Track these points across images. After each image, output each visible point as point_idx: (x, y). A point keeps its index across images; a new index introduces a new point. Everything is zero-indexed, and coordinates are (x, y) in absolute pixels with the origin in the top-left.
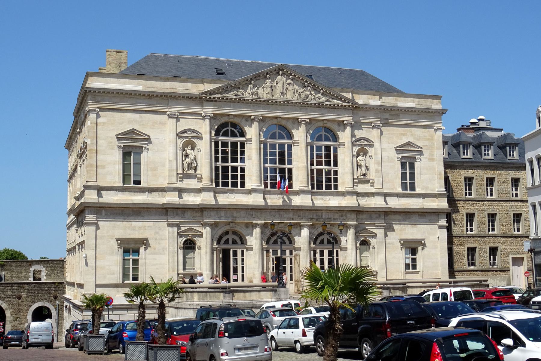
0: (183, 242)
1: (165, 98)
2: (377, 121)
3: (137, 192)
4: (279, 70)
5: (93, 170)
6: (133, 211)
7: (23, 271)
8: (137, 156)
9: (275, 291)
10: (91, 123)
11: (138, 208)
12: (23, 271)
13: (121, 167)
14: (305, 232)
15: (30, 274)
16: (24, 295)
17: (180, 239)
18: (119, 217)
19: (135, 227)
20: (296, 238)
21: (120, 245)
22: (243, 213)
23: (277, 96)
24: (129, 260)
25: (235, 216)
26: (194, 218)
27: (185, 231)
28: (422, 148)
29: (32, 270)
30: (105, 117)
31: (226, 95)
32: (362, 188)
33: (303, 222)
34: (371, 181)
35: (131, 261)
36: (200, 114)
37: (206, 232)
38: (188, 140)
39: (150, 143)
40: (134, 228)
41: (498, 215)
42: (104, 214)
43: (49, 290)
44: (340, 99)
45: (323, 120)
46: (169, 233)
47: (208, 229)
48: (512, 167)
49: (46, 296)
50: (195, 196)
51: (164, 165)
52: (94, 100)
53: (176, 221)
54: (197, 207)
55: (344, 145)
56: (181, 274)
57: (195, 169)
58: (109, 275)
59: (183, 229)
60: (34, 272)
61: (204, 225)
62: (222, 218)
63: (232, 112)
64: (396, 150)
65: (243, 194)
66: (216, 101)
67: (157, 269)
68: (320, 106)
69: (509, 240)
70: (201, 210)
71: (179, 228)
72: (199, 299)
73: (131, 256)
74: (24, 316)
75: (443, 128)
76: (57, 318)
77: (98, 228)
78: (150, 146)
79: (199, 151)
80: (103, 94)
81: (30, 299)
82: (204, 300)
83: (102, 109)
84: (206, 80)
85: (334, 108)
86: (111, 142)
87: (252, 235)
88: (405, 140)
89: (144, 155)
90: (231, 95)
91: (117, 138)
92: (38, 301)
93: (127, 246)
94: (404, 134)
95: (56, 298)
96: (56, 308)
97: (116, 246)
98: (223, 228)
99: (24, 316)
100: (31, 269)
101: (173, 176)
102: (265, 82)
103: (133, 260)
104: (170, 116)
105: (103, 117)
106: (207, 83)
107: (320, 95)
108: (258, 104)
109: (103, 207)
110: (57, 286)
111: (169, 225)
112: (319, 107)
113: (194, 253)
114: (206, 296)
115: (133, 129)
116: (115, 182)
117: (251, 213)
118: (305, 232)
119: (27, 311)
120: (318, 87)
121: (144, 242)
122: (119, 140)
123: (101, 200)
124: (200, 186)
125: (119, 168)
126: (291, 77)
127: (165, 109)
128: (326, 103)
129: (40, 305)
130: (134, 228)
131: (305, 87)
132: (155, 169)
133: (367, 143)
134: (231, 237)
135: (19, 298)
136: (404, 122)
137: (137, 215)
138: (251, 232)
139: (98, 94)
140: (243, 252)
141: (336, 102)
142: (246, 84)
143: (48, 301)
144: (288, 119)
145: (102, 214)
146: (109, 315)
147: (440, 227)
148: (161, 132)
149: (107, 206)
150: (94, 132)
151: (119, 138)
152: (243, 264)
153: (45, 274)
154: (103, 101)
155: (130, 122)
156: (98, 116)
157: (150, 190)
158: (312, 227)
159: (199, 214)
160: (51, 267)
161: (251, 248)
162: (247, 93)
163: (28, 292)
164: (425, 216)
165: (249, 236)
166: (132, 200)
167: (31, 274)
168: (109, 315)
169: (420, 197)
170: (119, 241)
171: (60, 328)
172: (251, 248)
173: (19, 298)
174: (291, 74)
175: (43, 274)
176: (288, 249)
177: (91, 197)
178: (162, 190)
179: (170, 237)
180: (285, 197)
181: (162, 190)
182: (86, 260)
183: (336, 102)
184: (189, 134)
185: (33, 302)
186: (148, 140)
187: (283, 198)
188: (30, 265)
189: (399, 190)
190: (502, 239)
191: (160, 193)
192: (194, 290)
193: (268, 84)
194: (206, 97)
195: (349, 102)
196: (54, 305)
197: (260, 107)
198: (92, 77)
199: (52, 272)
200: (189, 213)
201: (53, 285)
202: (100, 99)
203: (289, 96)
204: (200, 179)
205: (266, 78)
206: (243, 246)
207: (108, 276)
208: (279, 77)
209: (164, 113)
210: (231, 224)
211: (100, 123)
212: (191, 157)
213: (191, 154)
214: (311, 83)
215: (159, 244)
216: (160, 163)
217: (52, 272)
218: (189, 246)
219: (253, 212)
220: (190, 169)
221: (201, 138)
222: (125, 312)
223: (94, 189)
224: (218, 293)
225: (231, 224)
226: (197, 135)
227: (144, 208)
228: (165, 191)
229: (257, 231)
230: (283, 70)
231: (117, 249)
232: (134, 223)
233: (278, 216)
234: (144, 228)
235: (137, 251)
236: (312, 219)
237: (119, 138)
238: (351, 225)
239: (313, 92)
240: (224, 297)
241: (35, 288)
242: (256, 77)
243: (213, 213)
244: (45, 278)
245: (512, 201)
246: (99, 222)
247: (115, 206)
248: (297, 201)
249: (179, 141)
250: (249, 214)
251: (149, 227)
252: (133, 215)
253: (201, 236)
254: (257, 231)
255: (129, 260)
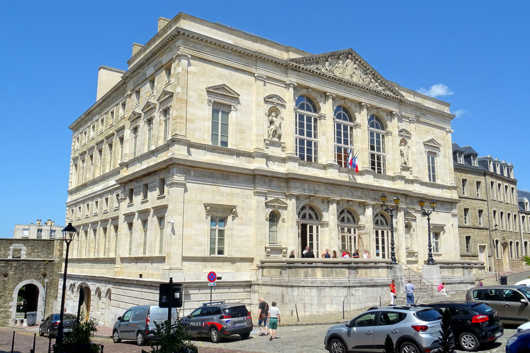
0: (269, 213)
1: (254, 59)
2: (412, 117)
3: (225, 154)
4: (349, 53)
5: (183, 123)
6: (222, 175)
7: (2, 249)
8: (225, 116)
9: (391, 268)
10: (182, 70)
11: (227, 172)
12: (2, 249)
13: (210, 124)
14: (369, 212)
15: (9, 252)
16: (11, 273)
17: (267, 210)
18: (208, 180)
19: (223, 193)
20: (361, 217)
21: (208, 212)
22: (322, 187)
23: (347, 77)
24: (215, 230)
25: (316, 189)
26: (280, 188)
27: (271, 202)
28: (440, 145)
29: (12, 248)
30: (197, 67)
31: (309, 67)
32: (406, 174)
33: (369, 201)
34: (410, 169)
35: (217, 231)
36: (284, 82)
37: (292, 204)
38: (274, 106)
39: (239, 103)
40: (222, 194)
41: (470, 210)
42: (192, 174)
43: (37, 268)
44: (392, 91)
45: (377, 108)
46: (258, 202)
47: (294, 200)
48: (476, 172)
49: (35, 274)
50: (279, 165)
51: (250, 129)
52: (186, 44)
53: (264, 190)
54: (285, 177)
55: (391, 134)
56: (268, 248)
57: (279, 137)
58: (196, 246)
59: (269, 199)
60: (14, 250)
61: (290, 197)
62: (306, 191)
63: (313, 85)
64: (424, 144)
65: (319, 168)
66: (299, 71)
67: (244, 241)
68: (377, 94)
69: (477, 231)
70: (288, 180)
71: (266, 199)
72: (323, 276)
73: (217, 226)
74: (9, 294)
75: (452, 131)
76: (44, 296)
77: (186, 191)
78: (238, 107)
79: (282, 118)
80: (196, 41)
81: (17, 276)
82: (329, 276)
83: (194, 57)
84: (291, 49)
85: (387, 97)
86: (201, 96)
87: (327, 211)
88: (429, 138)
89: (233, 115)
90: (313, 67)
91: (208, 91)
92: (25, 279)
93: (215, 214)
94: (428, 132)
95: (45, 275)
96: (44, 286)
97: (204, 212)
98: (304, 202)
99: (9, 294)
100: (10, 247)
101: (260, 141)
102: (337, 63)
103: (219, 231)
104: (257, 78)
105: (194, 65)
106: (291, 52)
107: (377, 84)
108: (333, 82)
109: (192, 167)
110: (47, 264)
111: (258, 194)
112: (376, 95)
113: (277, 226)
114: (332, 273)
115: (224, 85)
116: (204, 140)
117: (329, 188)
118: (369, 212)
119: (13, 289)
120: (377, 76)
121: (231, 210)
122: (210, 94)
123: (190, 158)
124: (284, 155)
125: (209, 124)
126: (357, 62)
127: (253, 70)
128: (383, 92)
129: (28, 283)
130: (222, 194)
131: (367, 74)
132: (242, 132)
133: (406, 135)
134: (307, 211)
135: (6, 275)
136: (428, 121)
137: (226, 179)
138: (326, 207)
139: (191, 39)
140: (317, 227)
141: (388, 93)
142: (323, 60)
143: (36, 279)
144: (352, 101)
145: (190, 175)
146: (211, 293)
147: (454, 215)
148: (252, 93)
149: (198, 165)
150: (185, 80)
151: (210, 92)
152: (317, 240)
153: (26, 252)
154: (195, 49)
155: (220, 77)
156: (189, 64)
157: (239, 154)
158: (374, 207)
159: (284, 185)
160: (32, 246)
161: (326, 224)
162: (325, 68)
163: (16, 269)
164: (444, 205)
165: (325, 212)
166: (221, 162)
167: (11, 253)
168: (211, 293)
169: (440, 188)
170: (208, 208)
171: (47, 306)
172: (326, 224)
173: (6, 275)
174: (357, 60)
175: (23, 252)
176: (352, 227)
177: (179, 152)
178: (249, 155)
179: (258, 207)
180: (351, 176)
181: (249, 155)
182: (173, 227)
183: (388, 93)
184: (274, 100)
185: (21, 280)
186: (236, 99)
187: (349, 177)
188: (10, 243)
189: (427, 180)
190: (473, 230)
191: (247, 158)
192: (311, 266)
193: (341, 65)
194: (293, 65)
195: (397, 95)
196: (42, 283)
197: (333, 85)
198: (184, 19)
199: (33, 250)
200: (275, 183)
201: (42, 262)
202: (191, 45)
203: (355, 80)
204: (284, 149)
205: (339, 58)
206: (318, 222)
207: (195, 248)
208: (348, 60)
209: (252, 74)
210: (312, 198)
211: (191, 72)
212: (277, 123)
213: (276, 121)
214: (371, 72)
215: (246, 213)
216: (248, 126)
217: (33, 250)
218: (274, 218)
219: (330, 187)
220: (275, 138)
221: (284, 106)
222: (227, 290)
223: (184, 145)
224: (344, 269)
225: (312, 198)
226: (281, 103)
227: (233, 172)
228: (253, 157)
229: (333, 208)
230: (352, 54)
231: (205, 216)
232: (222, 189)
233: (350, 193)
234: (232, 195)
235: (223, 220)
236: (375, 199)
237: (210, 92)
238: (402, 208)
239: (373, 80)
240: (349, 273)
241: (24, 266)
242: (331, 56)
243: (298, 185)
244: (25, 257)
245: (477, 199)
246: (187, 184)
247: (206, 166)
248: (360, 180)
249: (266, 105)
250: (328, 189)
251: (236, 194)
252: (222, 178)
253: (286, 208)
254: (333, 208)
255: (215, 230)
